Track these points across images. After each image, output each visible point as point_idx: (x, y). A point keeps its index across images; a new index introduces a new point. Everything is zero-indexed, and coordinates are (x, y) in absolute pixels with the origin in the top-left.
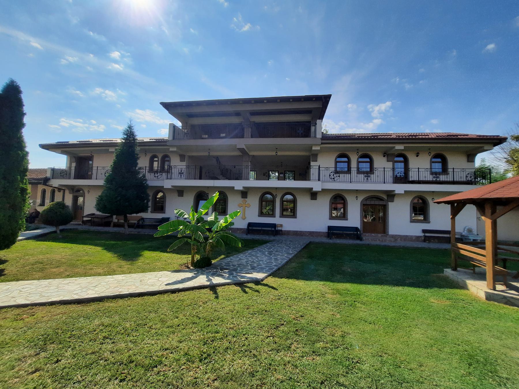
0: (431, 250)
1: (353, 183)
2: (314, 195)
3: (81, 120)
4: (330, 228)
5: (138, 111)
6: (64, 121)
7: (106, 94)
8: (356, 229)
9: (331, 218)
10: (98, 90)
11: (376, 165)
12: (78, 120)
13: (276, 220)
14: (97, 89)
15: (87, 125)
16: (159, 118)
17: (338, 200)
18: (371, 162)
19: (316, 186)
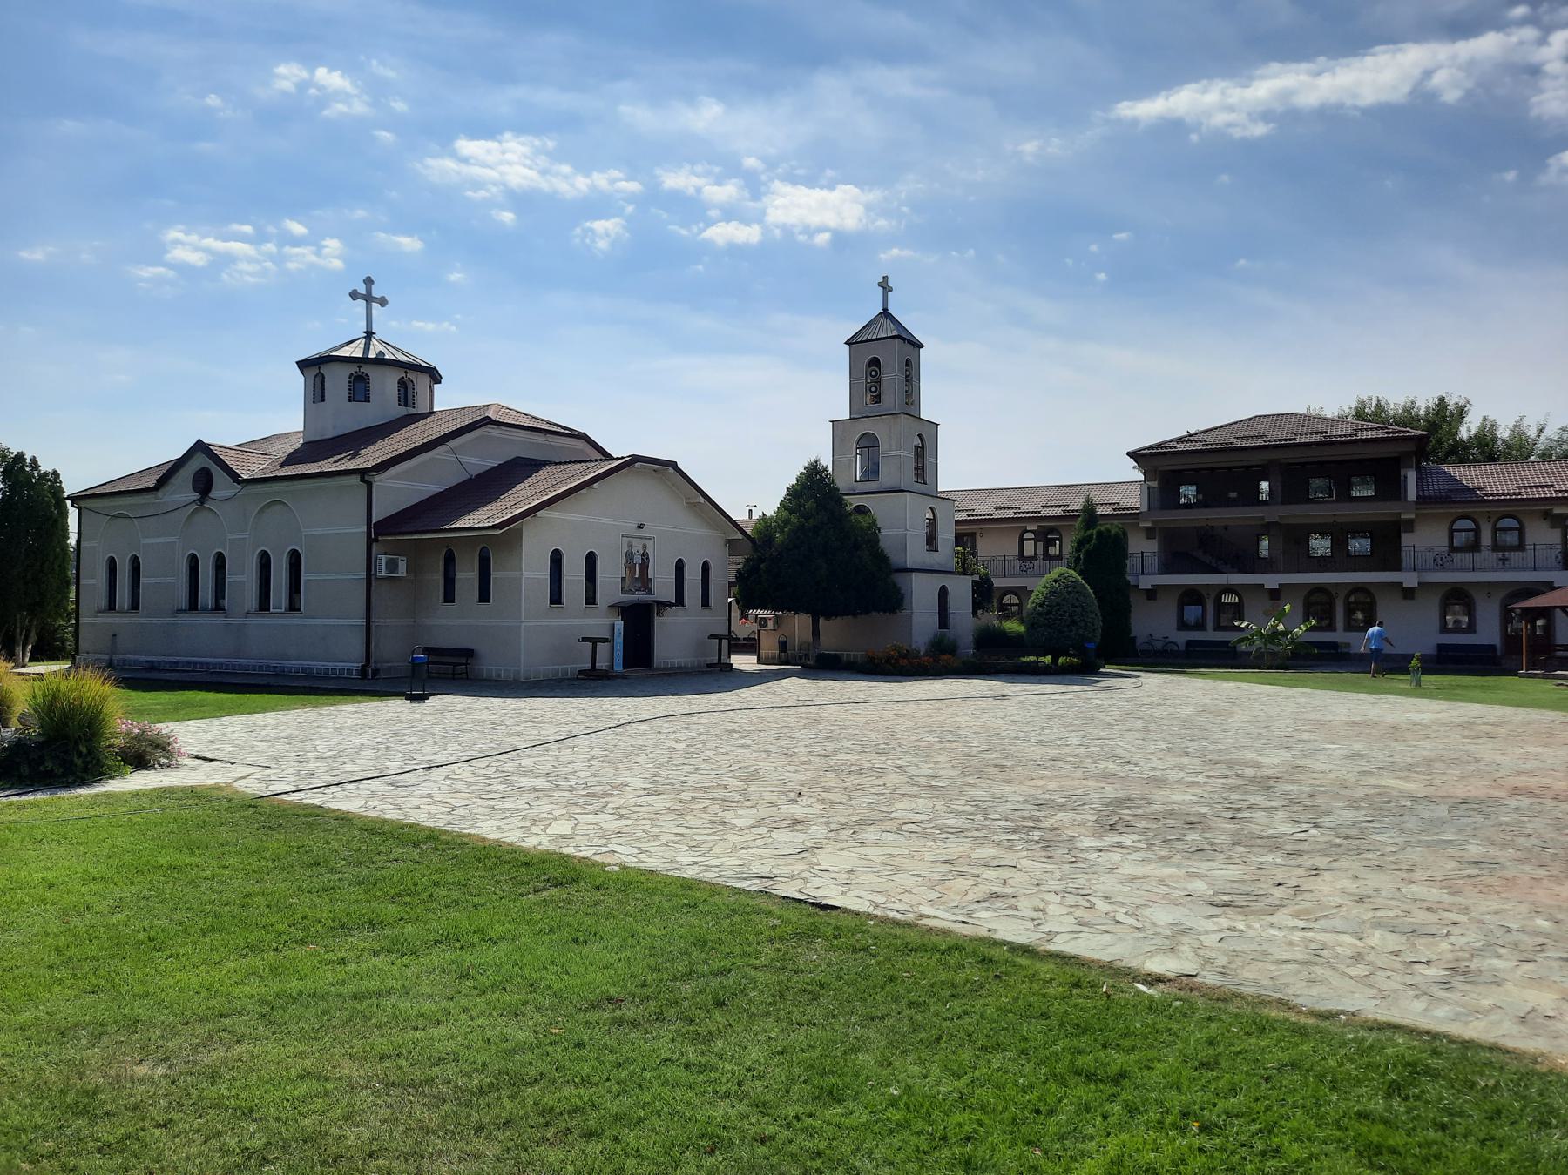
0: (416, 532)
1: (1483, 571)
2: (1408, 593)
3: (248, 229)
4: (1441, 647)
5: (466, 146)
6: (183, 244)
7: (321, 88)
8: (1493, 647)
9: (1444, 629)
10: (288, 74)
11: (1530, 539)
12: (235, 227)
13: (1339, 636)
14: (282, 69)
15: (270, 247)
16: (566, 169)
17: (1458, 596)
18: (1470, 612)
19: (1409, 579)
